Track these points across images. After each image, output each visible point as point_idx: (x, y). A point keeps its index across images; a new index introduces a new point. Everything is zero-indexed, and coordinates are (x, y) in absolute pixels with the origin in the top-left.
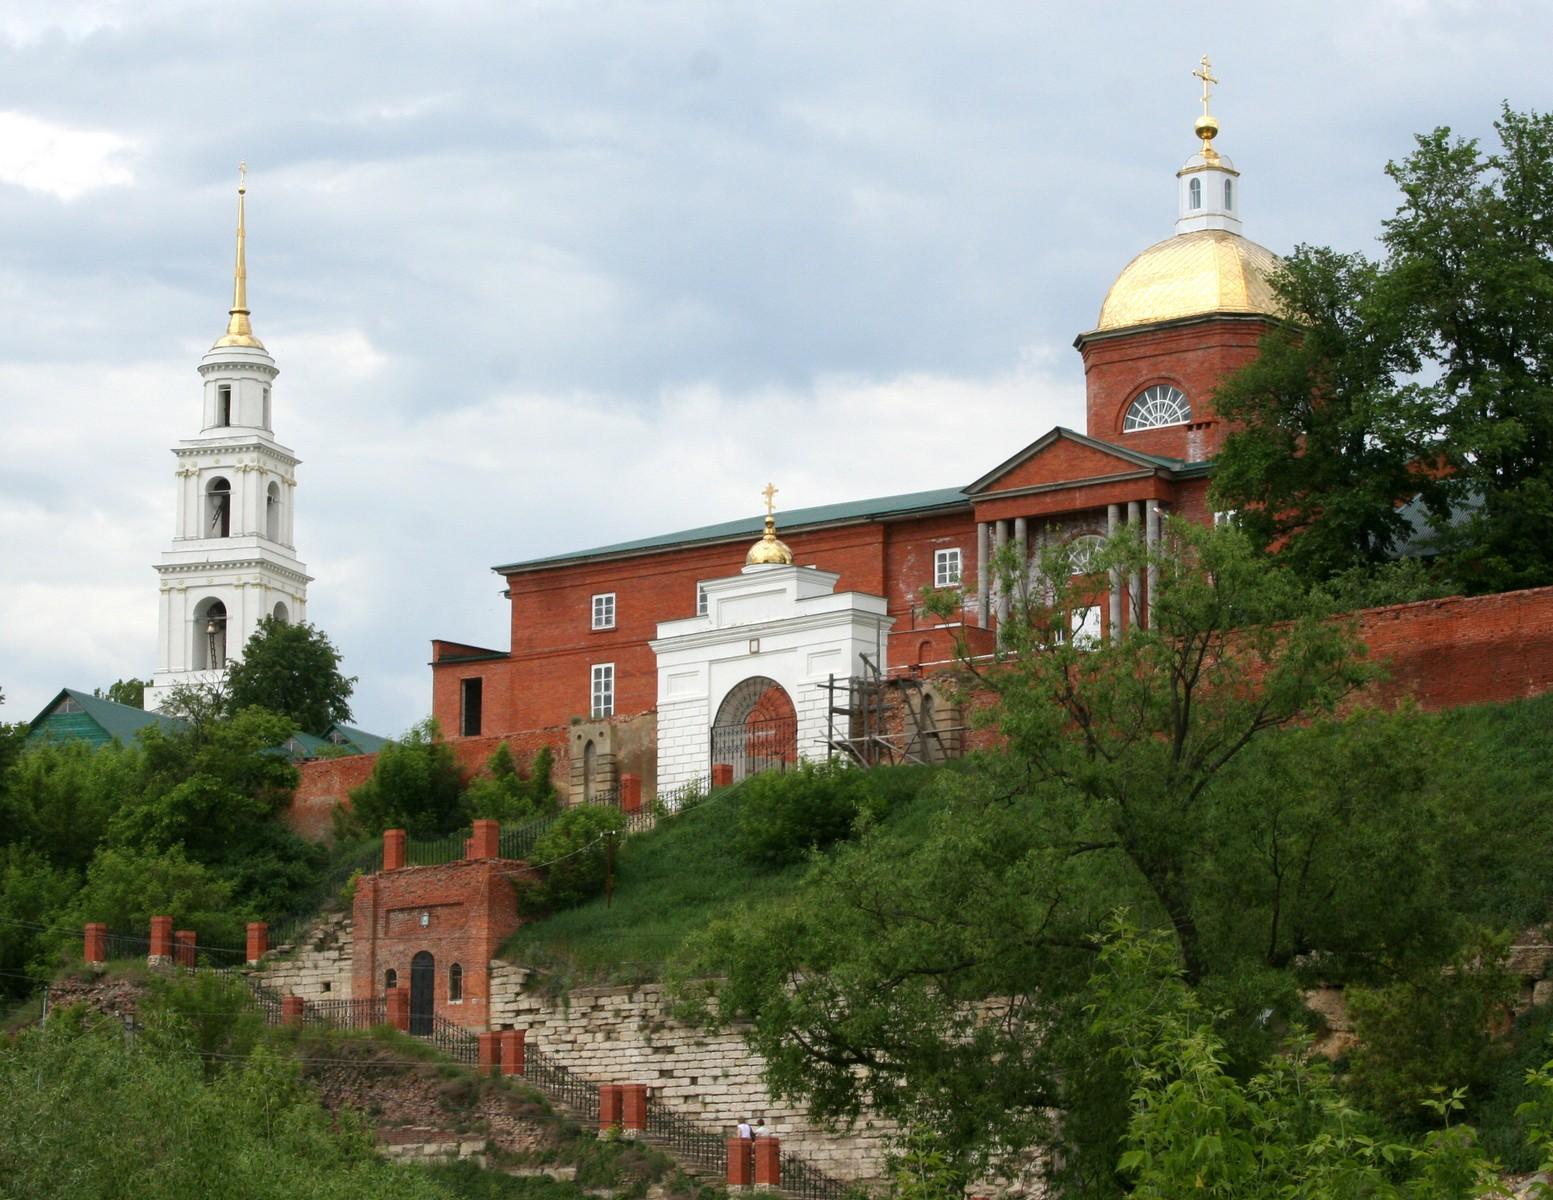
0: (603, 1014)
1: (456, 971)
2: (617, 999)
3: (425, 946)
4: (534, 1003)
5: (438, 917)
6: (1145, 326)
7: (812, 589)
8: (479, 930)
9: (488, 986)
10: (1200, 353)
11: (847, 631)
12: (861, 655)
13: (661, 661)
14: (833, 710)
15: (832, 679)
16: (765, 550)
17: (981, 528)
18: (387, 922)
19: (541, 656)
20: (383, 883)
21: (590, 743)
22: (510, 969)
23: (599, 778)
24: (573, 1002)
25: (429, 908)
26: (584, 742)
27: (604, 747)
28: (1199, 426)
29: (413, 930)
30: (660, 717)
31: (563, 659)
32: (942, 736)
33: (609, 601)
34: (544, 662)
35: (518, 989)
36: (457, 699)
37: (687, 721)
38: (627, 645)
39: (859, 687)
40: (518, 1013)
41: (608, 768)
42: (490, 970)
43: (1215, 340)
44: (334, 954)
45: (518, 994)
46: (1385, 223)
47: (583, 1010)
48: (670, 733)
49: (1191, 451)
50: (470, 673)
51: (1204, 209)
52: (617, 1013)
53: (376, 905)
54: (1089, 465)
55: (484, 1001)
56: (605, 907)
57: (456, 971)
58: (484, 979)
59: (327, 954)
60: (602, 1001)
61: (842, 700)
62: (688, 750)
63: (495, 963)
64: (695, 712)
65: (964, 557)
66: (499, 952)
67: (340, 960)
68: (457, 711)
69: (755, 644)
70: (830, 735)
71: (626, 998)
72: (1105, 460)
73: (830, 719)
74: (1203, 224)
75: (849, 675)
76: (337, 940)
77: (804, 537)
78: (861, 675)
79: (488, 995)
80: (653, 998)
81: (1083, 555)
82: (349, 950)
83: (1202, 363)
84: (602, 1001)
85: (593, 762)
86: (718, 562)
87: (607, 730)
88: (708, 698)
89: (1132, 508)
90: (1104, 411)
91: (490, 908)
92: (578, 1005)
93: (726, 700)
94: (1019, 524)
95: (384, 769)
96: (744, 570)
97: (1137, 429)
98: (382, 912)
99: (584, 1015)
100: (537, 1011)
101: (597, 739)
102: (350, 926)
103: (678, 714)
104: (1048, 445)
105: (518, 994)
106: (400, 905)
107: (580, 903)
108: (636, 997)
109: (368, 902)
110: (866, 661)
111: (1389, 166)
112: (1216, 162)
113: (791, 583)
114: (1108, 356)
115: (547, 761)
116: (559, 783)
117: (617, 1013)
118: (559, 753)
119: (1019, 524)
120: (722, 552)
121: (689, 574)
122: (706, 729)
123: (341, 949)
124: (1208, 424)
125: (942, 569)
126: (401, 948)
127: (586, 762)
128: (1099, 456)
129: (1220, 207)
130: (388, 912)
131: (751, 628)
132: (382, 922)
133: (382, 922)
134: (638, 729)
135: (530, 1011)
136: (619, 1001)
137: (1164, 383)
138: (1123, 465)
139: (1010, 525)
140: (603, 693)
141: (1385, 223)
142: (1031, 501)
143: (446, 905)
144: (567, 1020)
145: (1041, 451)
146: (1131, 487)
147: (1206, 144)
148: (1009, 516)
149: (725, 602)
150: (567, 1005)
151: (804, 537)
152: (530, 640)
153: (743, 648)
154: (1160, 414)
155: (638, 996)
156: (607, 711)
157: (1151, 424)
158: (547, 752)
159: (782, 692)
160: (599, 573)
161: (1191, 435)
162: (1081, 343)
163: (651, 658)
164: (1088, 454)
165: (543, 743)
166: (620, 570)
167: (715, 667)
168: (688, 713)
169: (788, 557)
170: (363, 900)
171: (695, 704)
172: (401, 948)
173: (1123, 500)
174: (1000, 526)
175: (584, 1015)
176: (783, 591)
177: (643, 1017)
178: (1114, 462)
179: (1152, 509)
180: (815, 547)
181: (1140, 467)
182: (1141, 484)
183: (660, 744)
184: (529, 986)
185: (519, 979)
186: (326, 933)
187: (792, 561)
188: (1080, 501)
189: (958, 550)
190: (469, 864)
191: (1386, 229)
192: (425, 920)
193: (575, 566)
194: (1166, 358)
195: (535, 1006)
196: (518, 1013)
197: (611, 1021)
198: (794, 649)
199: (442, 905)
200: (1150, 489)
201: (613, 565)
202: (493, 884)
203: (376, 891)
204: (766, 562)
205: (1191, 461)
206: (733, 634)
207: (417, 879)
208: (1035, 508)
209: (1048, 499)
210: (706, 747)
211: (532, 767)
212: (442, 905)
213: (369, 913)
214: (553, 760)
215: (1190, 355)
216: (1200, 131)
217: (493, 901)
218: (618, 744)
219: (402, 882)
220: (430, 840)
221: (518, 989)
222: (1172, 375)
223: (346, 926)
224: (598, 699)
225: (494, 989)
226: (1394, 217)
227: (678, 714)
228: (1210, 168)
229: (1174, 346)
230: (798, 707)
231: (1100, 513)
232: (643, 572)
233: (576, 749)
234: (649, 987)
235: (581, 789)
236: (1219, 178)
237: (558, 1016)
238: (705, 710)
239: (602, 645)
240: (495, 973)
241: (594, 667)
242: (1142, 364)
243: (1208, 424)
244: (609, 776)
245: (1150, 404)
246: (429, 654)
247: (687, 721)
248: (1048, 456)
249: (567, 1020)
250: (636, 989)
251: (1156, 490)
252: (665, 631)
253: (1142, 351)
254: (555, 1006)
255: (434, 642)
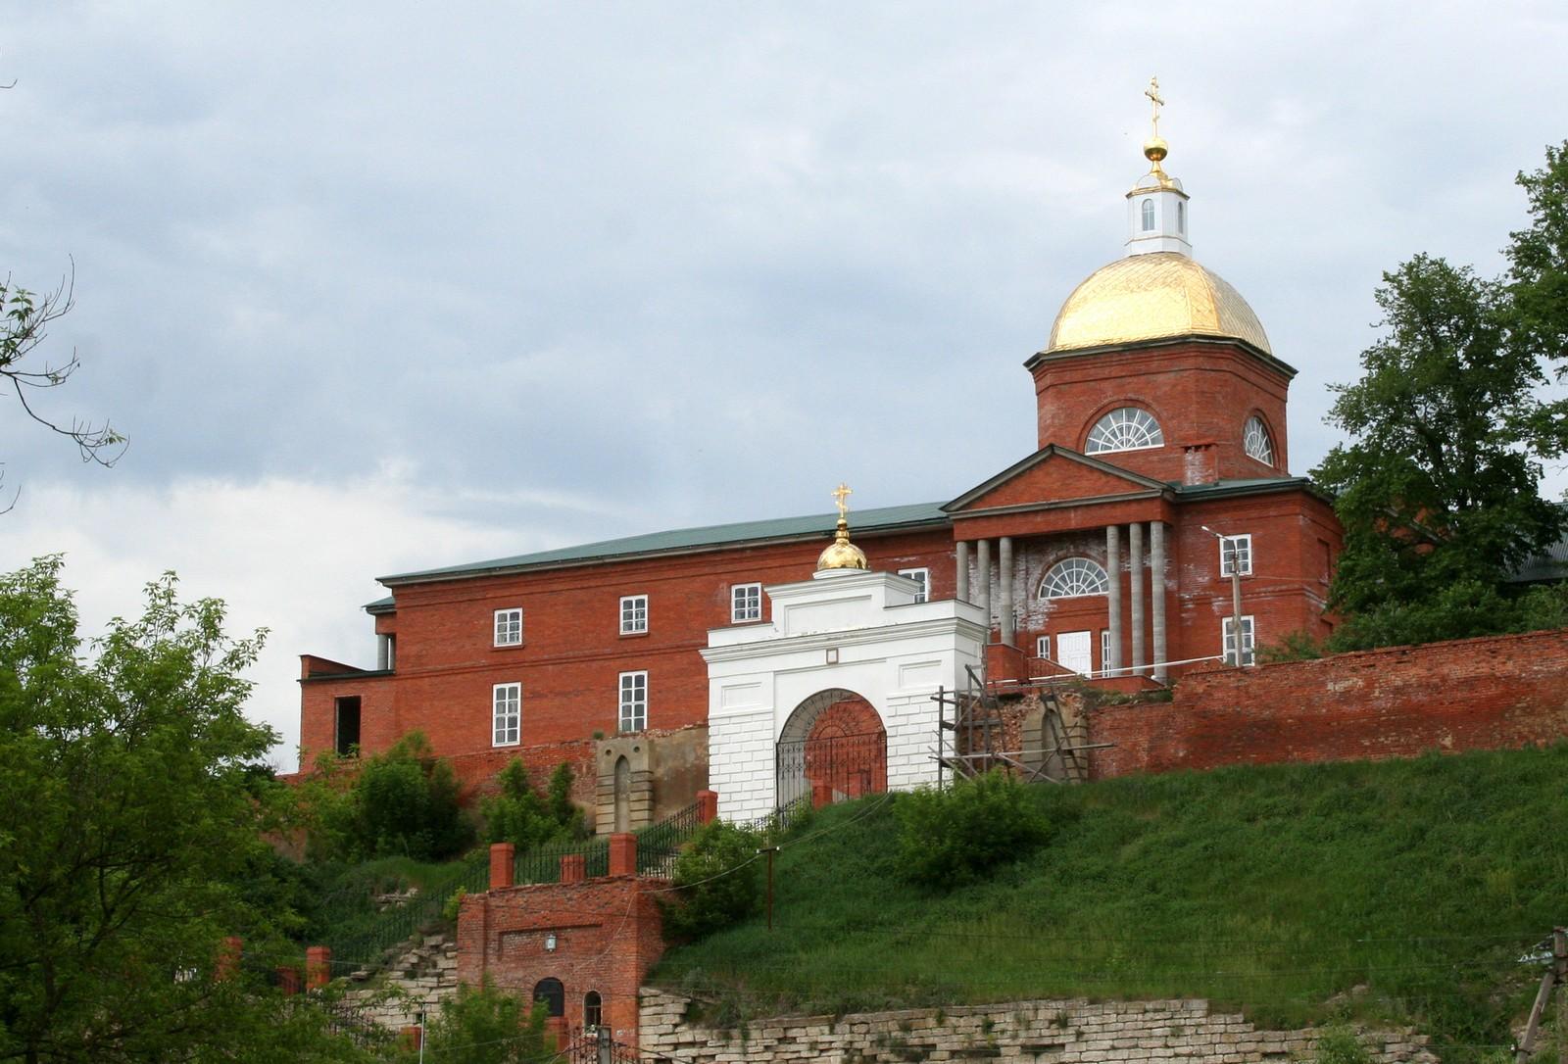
0: (793, 1047)
1: (593, 999)
2: (813, 1031)
3: (552, 970)
4: (699, 1035)
5: (567, 940)
6: (1112, 345)
7: (899, 598)
8: (626, 956)
9: (638, 1016)
10: (1172, 375)
11: (950, 641)
12: (967, 667)
13: (713, 671)
14: (943, 725)
15: (942, 692)
16: (839, 554)
17: (961, 547)
18: (501, 948)
19: (431, 674)
20: (494, 902)
21: (622, 758)
22: (665, 998)
23: (634, 796)
24: (755, 1034)
25: (556, 930)
26: (614, 758)
27: (641, 763)
28: (1197, 448)
29: (539, 952)
30: (711, 731)
31: (459, 677)
32: (1077, 753)
33: (515, 616)
34: (436, 680)
35: (677, 1019)
36: (330, 718)
37: (747, 737)
38: (534, 664)
39: (962, 701)
40: (676, 1046)
41: (646, 786)
42: (639, 999)
43: (1190, 363)
44: (432, 981)
45: (676, 1026)
46: (1513, 235)
47: (768, 1042)
48: (725, 749)
49: (1189, 474)
50: (347, 691)
51: (1158, 230)
52: (813, 1046)
53: (487, 926)
54: (1085, 484)
55: (633, 1031)
56: (765, 930)
57: (593, 999)
58: (632, 1010)
59: (422, 982)
60: (792, 1033)
61: (950, 714)
62: (747, 767)
63: (644, 991)
64: (757, 725)
65: (933, 577)
66: (649, 977)
67: (439, 987)
68: (331, 732)
69: (832, 654)
70: (941, 751)
71: (826, 1029)
72: (1104, 479)
73: (941, 735)
74: (1158, 245)
75: (953, 689)
76: (435, 966)
77: (748, 553)
78: (966, 687)
79: (637, 1025)
80: (863, 1028)
81: (1087, 578)
82: (451, 977)
83: (1174, 386)
84: (792, 1033)
85: (626, 780)
86: (646, 577)
87: (644, 747)
88: (773, 712)
89: (1134, 531)
90: (1064, 433)
91: (639, 930)
92: (759, 1038)
93: (795, 714)
94: (1004, 544)
95: (373, 785)
96: (816, 575)
97: (1100, 452)
98: (493, 934)
99: (767, 1048)
100: (704, 1044)
101: (630, 755)
102: (452, 950)
103: (732, 729)
104: (1039, 463)
105: (676, 1026)
106: (519, 927)
107: (727, 927)
108: (838, 1028)
109: (477, 923)
110: (971, 674)
111: (1520, 176)
112: (1170, 184)
113: (877, 589)
114: (1068, 376)
115: (565, 778)
116: (580, 802)
117: (813, 1046)
118: (580, 770)
119: (1004, 544)
120: (789, 553)
121: (612, 589)
122: (771, 745)
123: (440, 975)
124: (1208, 446)
125: (629, 616)
126: (520, 974)
127: (617, 779)
128: (1096, 475)
129: (1174, 231)
130: (502, 934)
131: (829, 637)
132: (494, 945)
133: (494, 945)
134: (679, 745)
135: (692, 1044)
136: (819, 1032)
137: (1132, 404)
138: (1124, 484)
139: (993, 544)
140: (507, 716)
141: (1513, 235)
142: (1019, 520)
143: (579, 927)
144: (745, 1054)
145: (1030, 468)
146: (1134, 507)
147: (1155, 165)
148: (992, 534)
149: (796, 609)
150: (746, 1037)
151: (748, 553)
152: (419, 657)
153: (819, 658)
154: (1125, 435)
155: (842, 1027)
156: (639, 723)
157: (1117, 447)
158: (565, 768)
159: (863, 703)
160: (733, 561)
161: (1189, 457)
162: (1038, 365)
163: (702, 668)
164: (1085, 472)
165: (559, 759)
166: (528, 584)
167: (781, 679)
168: (746, 727)
169: (864, 561)
170: (471, 918)
171: (756, 718)
172: (520, 974)
173: (1124, 521)
174: (982, 546)
175: (767, 1048)
176: (868, 597)
177: (846, 1051)
178: (1113, 482)
179: (1156, 531)
180: (760, 564)
181: (1145, 487)
182: (1144, 504)
183: (712, 760)
184: (690, 1017)
185: (681, 1009)
186: (421, 957)
187: (867, 565)
188: (1075, 521)
189: (925, 570)
190: (611, 881)
191: (1512, 241)
192: (551, 943)
193: (474, 579)
194: (1135, 380)
195: (700, 1038)
196: (676, 1046)
197: (804, 1054)
198: (883, 660)
199: (573, 927)
200: (1155, 511)
201: (521, 579)
202: (642, 903)
203: (487, 910)
204: (843, 566)
205: (1189, 484)
206: (806, 642)
207: (538, 898)
208: (1024, 528)
209: (1039, 519)
210: (772, 764)
211: (546, 784)
212: (573, 927)
213: (478, 935)
214: (573, 777)
215: (1161, 378)
216: (1149, 153)
217: (642, 921)
218: (656, 760)
219: (520, 900)
220: (422, 860)
221: (677, 1019)
222: (1141, 398)
223: (445, 952)
224: (501, 721)
225: (644, 1020)
226: (1532, 227)
227: (732, 729)
228: (1165, 189)
229: (1143, 367)
230: (887, 723)
231: (1099, 535)
232: (555, 587)
233: (604, 765)
234: (856, 1017)
235: (611, 809)
236: (1174, 199)
237: (732, 1049)
238: (770, 724)
239: (635, 651)
240: (646, 1001)
241: (496, 687)
242: (1105, 385)
243: (1208, 446)
244: (647, 795)
245: (1134, 424)
246: (297, 671)
247: (747, 737)
248: (1038, 474)
249: (745, 1054)
250: (838, 1020)
251: (1162, 512)
252: (716, 638)
253: (1106, 372)
254: (728, 1037)
255: (302, 657)
